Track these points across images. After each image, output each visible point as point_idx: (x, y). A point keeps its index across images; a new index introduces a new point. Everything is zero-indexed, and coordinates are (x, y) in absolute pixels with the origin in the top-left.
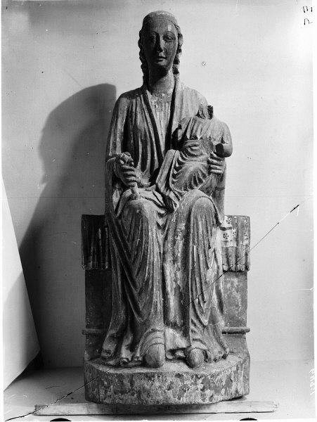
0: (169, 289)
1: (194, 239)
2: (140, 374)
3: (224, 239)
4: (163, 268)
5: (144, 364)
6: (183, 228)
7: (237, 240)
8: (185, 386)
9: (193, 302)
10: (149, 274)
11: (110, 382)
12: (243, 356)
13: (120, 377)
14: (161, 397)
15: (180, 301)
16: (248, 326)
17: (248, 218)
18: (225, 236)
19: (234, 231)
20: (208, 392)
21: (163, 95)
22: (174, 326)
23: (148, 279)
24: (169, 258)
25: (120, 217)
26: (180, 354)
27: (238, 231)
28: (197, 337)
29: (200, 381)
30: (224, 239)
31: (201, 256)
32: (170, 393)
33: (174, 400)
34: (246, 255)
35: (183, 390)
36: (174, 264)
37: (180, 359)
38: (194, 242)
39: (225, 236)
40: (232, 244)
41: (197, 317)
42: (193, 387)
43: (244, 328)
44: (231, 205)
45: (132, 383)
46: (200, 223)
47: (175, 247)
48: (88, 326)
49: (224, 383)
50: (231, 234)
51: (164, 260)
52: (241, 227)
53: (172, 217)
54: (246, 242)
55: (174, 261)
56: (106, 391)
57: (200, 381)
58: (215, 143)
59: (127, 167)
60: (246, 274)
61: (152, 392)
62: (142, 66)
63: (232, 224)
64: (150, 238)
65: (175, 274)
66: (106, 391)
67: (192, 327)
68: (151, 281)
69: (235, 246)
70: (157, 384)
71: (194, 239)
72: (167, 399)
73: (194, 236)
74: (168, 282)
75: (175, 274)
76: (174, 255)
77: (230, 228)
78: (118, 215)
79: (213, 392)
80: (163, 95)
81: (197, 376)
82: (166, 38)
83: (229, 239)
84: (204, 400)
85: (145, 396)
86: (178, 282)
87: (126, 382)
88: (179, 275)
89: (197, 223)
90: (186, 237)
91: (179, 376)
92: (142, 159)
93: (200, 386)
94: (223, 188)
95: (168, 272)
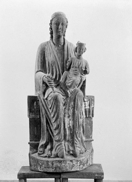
0: (66, 127)
1: (76, 108)
2: (56, 161)
3: (85, 106)
4: (64, 119)
5: (57, 156)
6: (73, 104)
7: (89, 105)
8: (74, 165)
9: (76, 132)
10: (59, 122)
11: (43, 164)
12: (91, 150)
13: (48, 162)
14: (64, 169)
15: (70, 132)
16: (93, 138)
17: (93, 97)
18: (85, 104)
19: (89, 102)
20: (81, 166)
21: (60, 46)
22: (68, 141)
23: (59, 124)
24: (67, 116)
25: (47, 99)
26: (71, 152)
27: (90, 102)
28: (77, 146)
29: (79, 162)
30: (85, 106)
31: (79, 114)
32: (68, 168)
33: (70, 170)
34: (93, 111)
35: (73, 166)
36: (68, 118)
37: (71, 154)
38: (76, 110)
39: (85, 104)
40: (87, 107)
41: (77, 138)
42: (76, 165)
43: (91, 139)
44: (88, 92)
45: (53, 164)
46: (79, 102)
47: (69, 111)
48: (30, 141)
49: (86, 162)
50: (87, 103)
51: (64, 116)
52: (91, 100)
53: (68, 100)
54: (92, 106)
55: (69, 117)
56: (41, 167)
57: (79, 162)
58: (84, 69)
59: (51, 80)
60: (92, 118)
61: (61, 168)
62: (50, 33)
63: (88, 99)
64: (60, 108)
65: (69, 122)
66: (41, 167)
67: (75, 142)
68: (60, 125)
69: (89, 108)
70: (63, 164)
71: (76, 108)
72: (66, 169)
73: (76, 107)
74: (66, 125)
75: (69, 122)
76: (68, 114)
77: (87, 101)
78: (46, 97)
79: (83, 166)
80: (60, 46)
81: (78, 160)
82: (62, 24)
83: (87, 105)
84: (80, 169)
85: (58, 169)
86: (70, 125)
87: (50, 164)
88: (71, 122)
89: (78, 102)
90: (74, 108)
91: (71, 161)
92: (59, 77)
93: (79, 164)
94: (85, 86)
95: (66, 121)
